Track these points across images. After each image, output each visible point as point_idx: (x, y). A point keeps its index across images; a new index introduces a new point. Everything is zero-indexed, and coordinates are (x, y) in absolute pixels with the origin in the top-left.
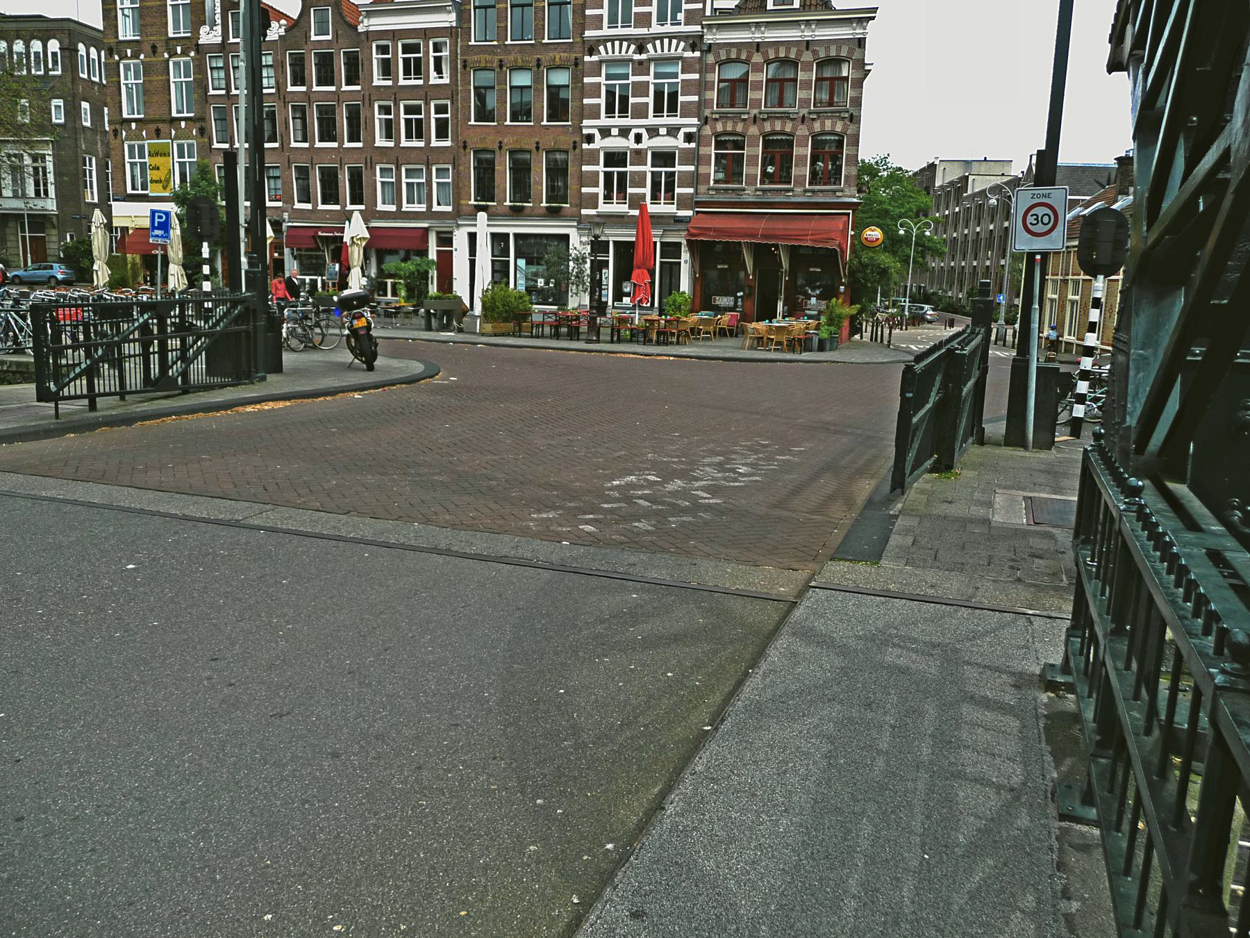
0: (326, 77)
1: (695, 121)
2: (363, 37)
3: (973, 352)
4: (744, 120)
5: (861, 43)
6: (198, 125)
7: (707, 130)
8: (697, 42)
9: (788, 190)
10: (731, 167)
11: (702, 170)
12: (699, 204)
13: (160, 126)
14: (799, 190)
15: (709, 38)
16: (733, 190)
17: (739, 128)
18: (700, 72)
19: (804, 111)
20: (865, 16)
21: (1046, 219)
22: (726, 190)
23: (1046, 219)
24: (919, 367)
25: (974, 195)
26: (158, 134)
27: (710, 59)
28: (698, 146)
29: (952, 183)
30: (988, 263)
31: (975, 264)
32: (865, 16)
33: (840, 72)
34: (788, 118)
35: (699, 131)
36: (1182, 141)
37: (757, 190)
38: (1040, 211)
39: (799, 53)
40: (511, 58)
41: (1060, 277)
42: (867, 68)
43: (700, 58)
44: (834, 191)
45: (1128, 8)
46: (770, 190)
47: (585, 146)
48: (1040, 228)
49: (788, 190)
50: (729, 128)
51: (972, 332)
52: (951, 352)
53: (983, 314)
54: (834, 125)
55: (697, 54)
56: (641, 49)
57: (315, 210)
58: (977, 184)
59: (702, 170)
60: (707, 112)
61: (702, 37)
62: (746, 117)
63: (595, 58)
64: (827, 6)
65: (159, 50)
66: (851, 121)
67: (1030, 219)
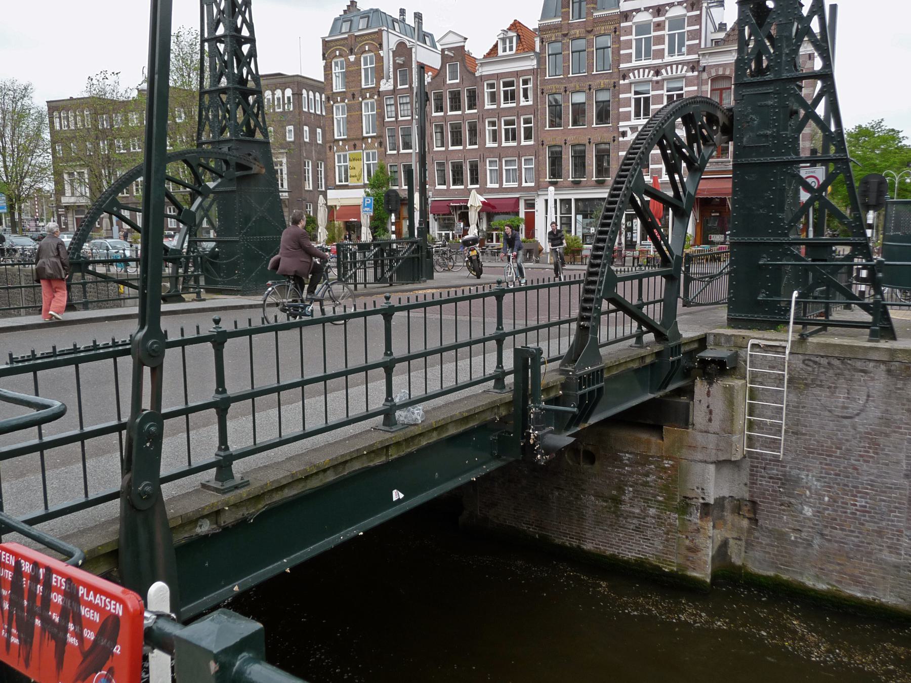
2: (479, 79)
6: (379, 140)
13: (356, 142)
26: (355, 147)
40: (572, 85)
47: (621, 139)
56: (657, 73)
57: (448, 189)
63: (627, 81)
65: (356, 96)
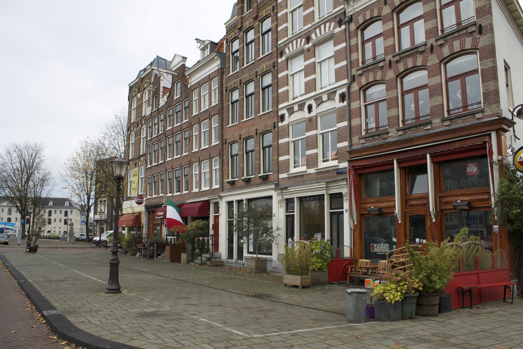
4: (422, 52)
59: (355, 122)
62: (381, 65)
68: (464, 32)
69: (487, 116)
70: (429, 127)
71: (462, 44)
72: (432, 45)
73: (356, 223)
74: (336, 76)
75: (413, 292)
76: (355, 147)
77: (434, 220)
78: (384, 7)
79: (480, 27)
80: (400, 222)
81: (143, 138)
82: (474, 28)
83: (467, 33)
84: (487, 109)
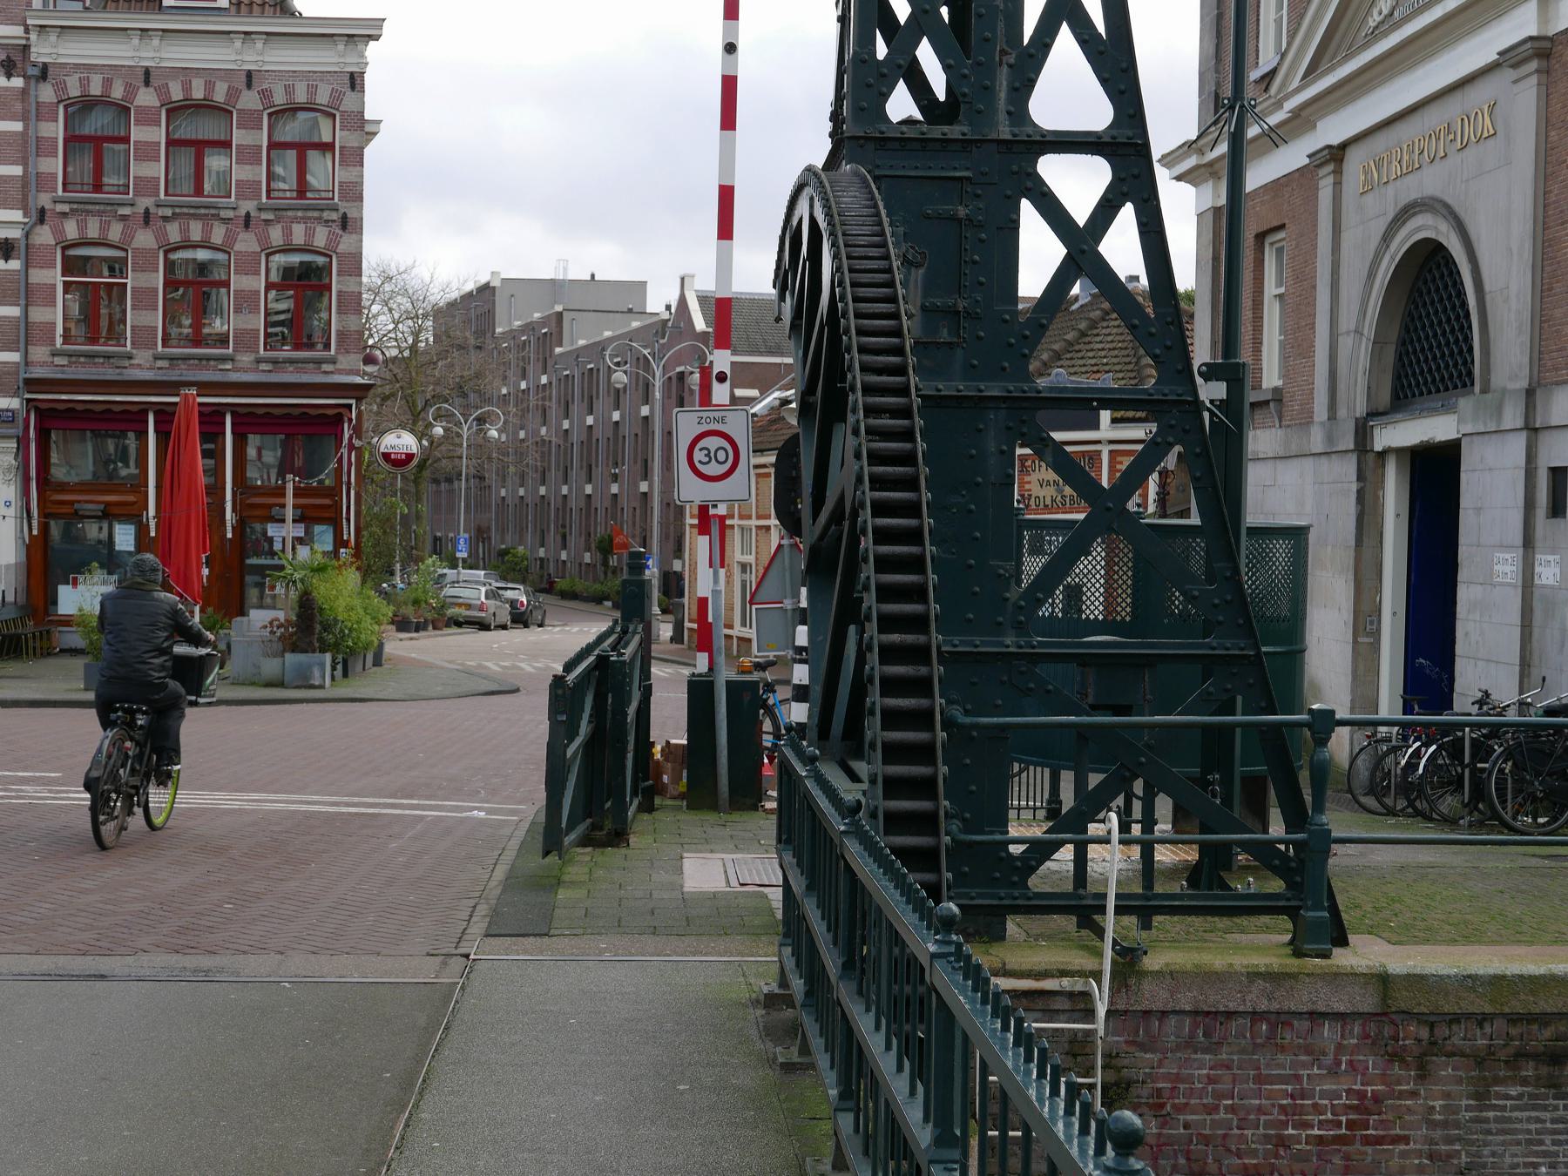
0: (922, 686)
1: (17, 215)
3: (633, 659)
4: (124, 218)
5: (355, 81)
7: (44, 236)
8: (17, 58)
9: (224, 359)
10: (97, 311)
11: (38, 314)
12: (32, 384)
14: (246, 358)
15: (43, 51)
16: (108, 357)
17: (115, 232)
18: (24, 118)
19: (248, 206)
20: (361, 33)
21: (721, 456)
22: (91, 356)
23: (721, 456)
24: (571, 678)
25: (577, 353)
27: (47, 93)
28: (27, 266)
29: (529, 327)
30: (615, 489)
31: (589, 489)
32: (361, 33)
33: (318, 127)
34: (217, 217)
35: (27, 235)
36: (1101, 28)
37: (157, 358)
38: (713, 443)
39: (233, 94)
41: (754, 522)
42: (368, 128)
43: (24, 92)
44: (319, 362)
45: (786, 272)
46: (185, 358)
48: (713, 469)
49: (224, 359)
50: (93, 232)
51: (625, 632)
52: (602, 661)
53: (631, 605)
54: (310, 233)
55: (17, 82)
58: (578, 338)
59: (38, 314)
60: (44, 200)
61: (26, 48)
62: (126, 211)
64: (282, 6)
66: (344, 227)
67: (698, 456)
68: (316, 214)
69: (340, 372)
70: (229, 366)
71: (104, 228)
72: (248, 215)
73: (35, 532)
74: (1141, 233)
75: (1276, 1111)
76: (38, 373)
77: (229, 535)
78: (245, 92)
79: (344, 217)
80: (153, 534)
81: (1298, 1078)
82: (334, 216)
83: (320, 218)
84: (340, 358)
